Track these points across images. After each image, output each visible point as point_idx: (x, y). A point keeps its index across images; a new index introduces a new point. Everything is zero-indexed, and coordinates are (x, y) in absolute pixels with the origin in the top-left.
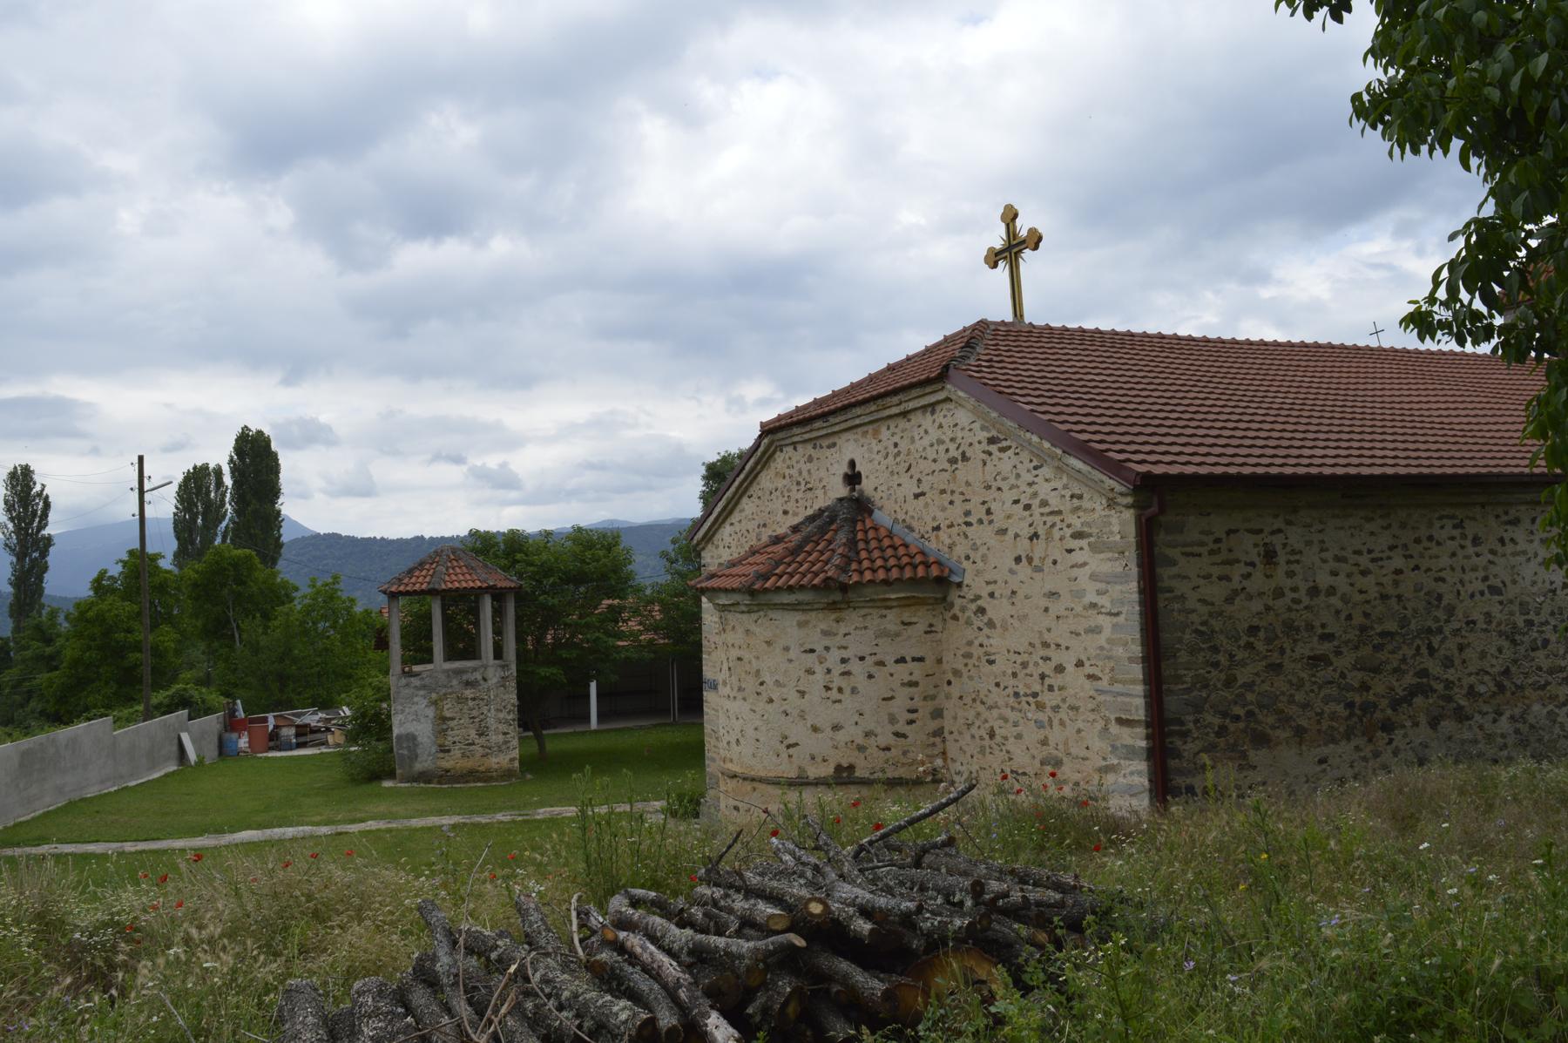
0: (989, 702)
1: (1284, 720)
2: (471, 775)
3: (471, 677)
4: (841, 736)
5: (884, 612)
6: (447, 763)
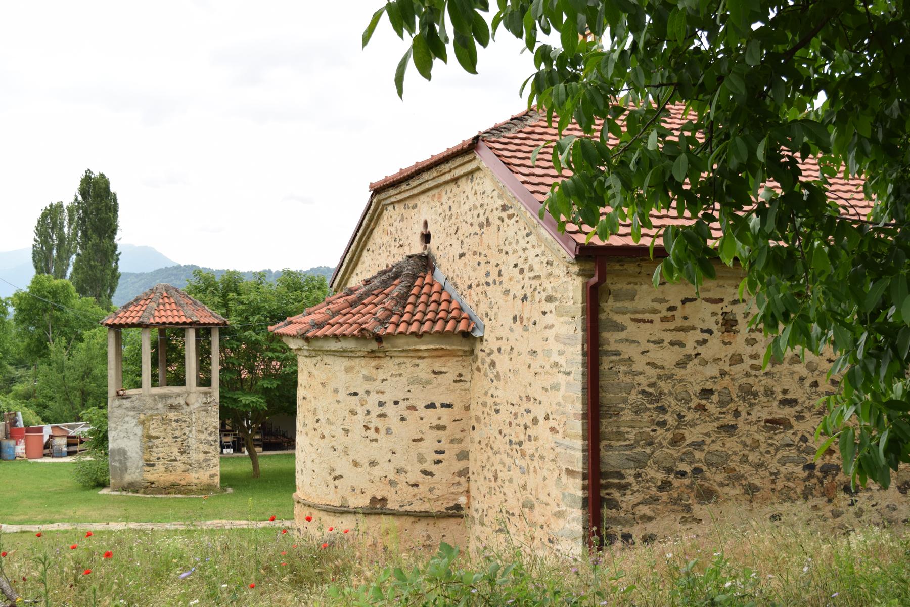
0: (496, 448)
1: (734, 477)
2: (173, 488)
3: (175, 402)
4: (377, 472)
5: (417, 361)
6: (152, 476)
